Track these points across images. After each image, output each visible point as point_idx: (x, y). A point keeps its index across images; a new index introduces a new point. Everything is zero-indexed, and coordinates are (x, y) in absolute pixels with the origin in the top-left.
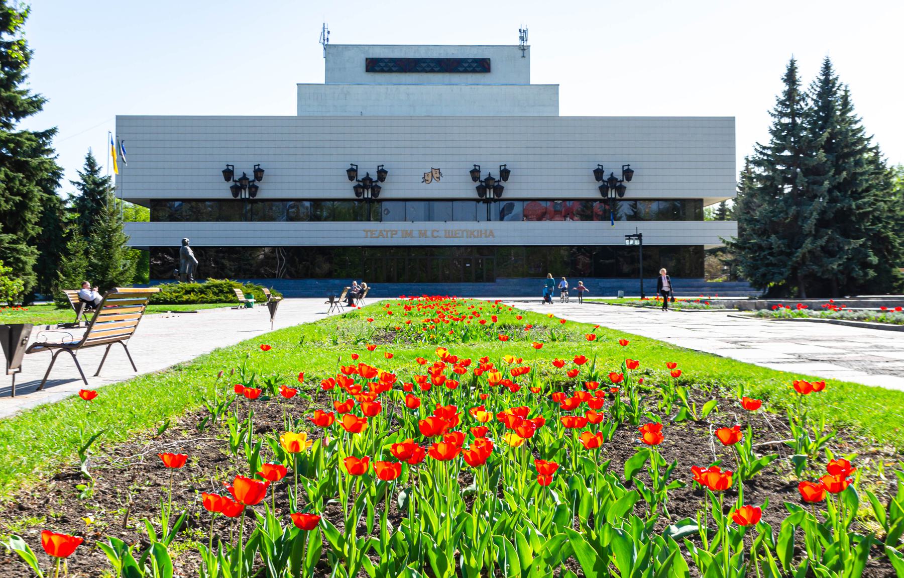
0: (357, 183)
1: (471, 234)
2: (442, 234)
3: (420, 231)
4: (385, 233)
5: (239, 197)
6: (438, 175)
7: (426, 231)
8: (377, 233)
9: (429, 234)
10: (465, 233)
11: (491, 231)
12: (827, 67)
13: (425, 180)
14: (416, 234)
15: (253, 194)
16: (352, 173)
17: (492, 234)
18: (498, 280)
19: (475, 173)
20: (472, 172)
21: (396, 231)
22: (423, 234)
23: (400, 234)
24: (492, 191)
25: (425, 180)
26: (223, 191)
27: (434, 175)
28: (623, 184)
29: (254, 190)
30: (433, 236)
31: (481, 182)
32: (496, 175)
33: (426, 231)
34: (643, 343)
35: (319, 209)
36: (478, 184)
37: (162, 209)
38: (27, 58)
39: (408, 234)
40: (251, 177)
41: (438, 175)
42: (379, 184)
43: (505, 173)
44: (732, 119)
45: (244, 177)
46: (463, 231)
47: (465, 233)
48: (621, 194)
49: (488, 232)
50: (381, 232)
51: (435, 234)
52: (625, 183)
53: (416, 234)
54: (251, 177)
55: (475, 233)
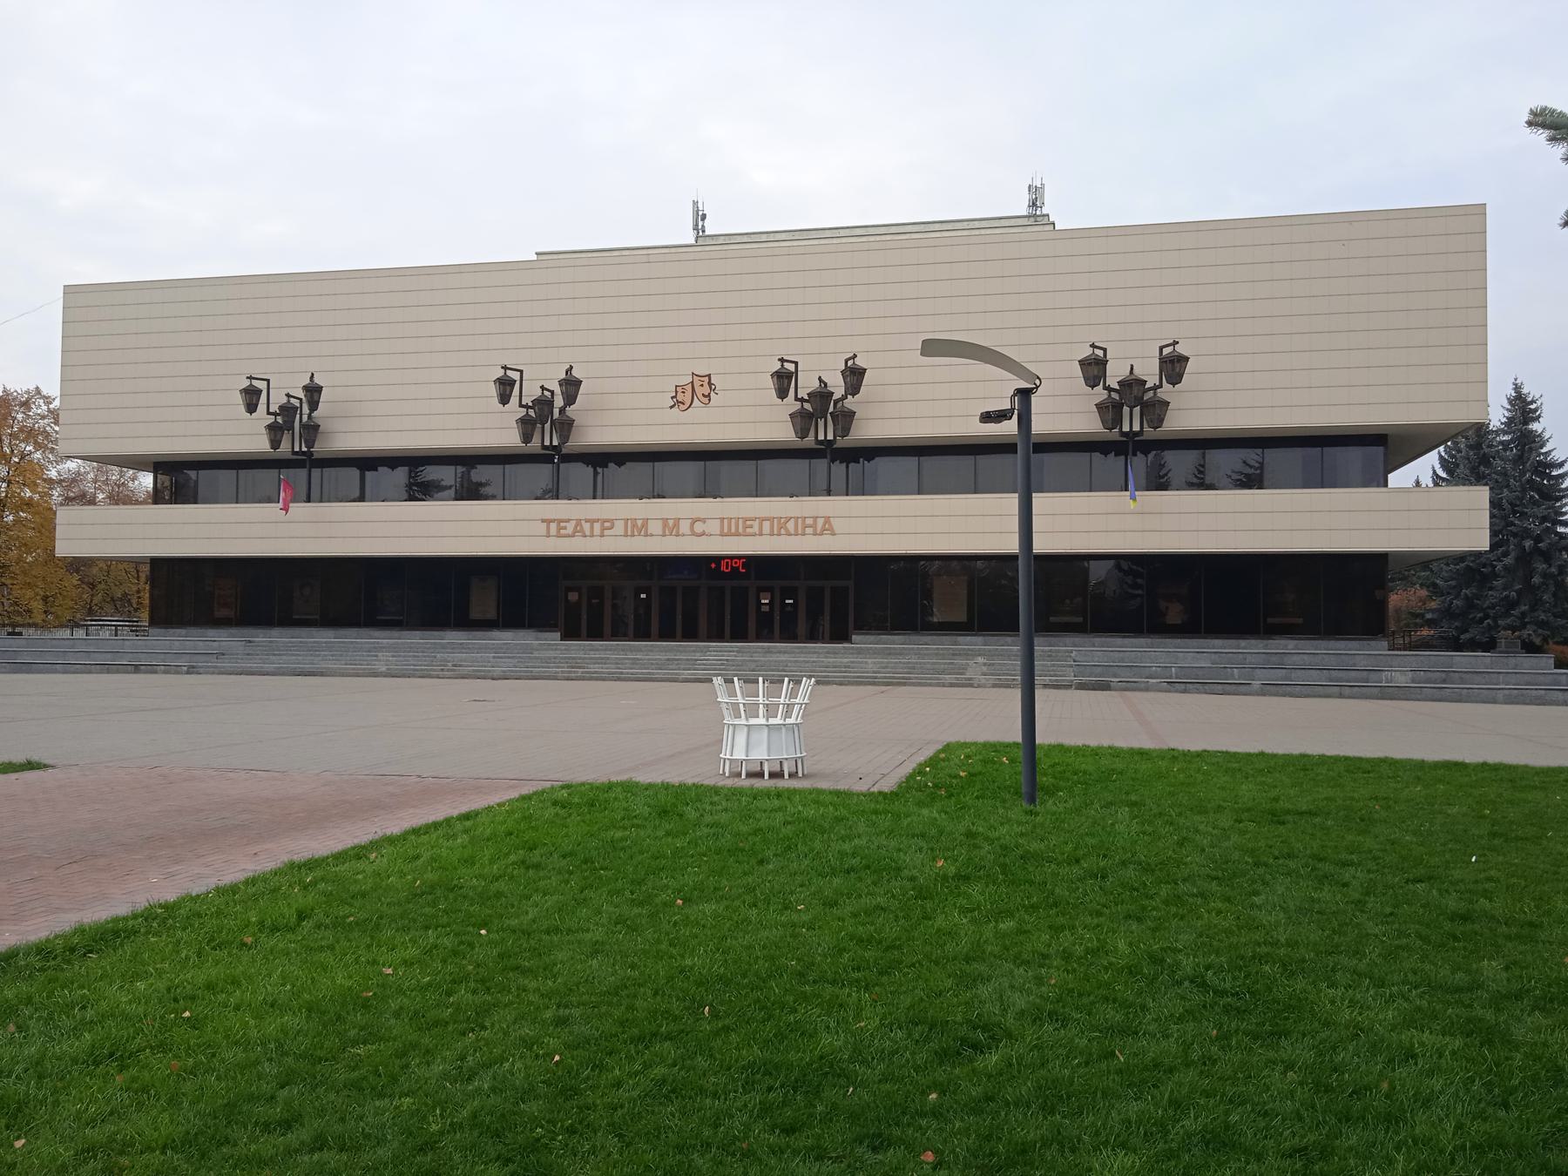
0: (798, 405)
4: (587, 526)
5: (811, 437)
6: (706, 390)
8: (570, 527)
9: (685, 527)
10: (766, 525)
12: (695, 203)
13: (677, 403)
15: (565, 438)
17: (828, 529)
21: (612, 521)
23: (619, 528)
24: (1137, 410)
25: (677, 403)
26: (250, 437)
27: (698, 390)
28: (1161, 394)
30: (694, 534)
31: (1109, 389)
32: (1149, 371)
34: (459, 826)
35: (420, 474)
36: (1100, 394)
37: (181, 479)
39: (638, 528)
40: (837, 386)
41: (706, 390)
42: (850, 402)
44: (1478, 212)
46: (592, 522)
47: (766, 525)
49: (820, 522)
50: (579, 522)
51: (699, 527)
54: (837, 386)
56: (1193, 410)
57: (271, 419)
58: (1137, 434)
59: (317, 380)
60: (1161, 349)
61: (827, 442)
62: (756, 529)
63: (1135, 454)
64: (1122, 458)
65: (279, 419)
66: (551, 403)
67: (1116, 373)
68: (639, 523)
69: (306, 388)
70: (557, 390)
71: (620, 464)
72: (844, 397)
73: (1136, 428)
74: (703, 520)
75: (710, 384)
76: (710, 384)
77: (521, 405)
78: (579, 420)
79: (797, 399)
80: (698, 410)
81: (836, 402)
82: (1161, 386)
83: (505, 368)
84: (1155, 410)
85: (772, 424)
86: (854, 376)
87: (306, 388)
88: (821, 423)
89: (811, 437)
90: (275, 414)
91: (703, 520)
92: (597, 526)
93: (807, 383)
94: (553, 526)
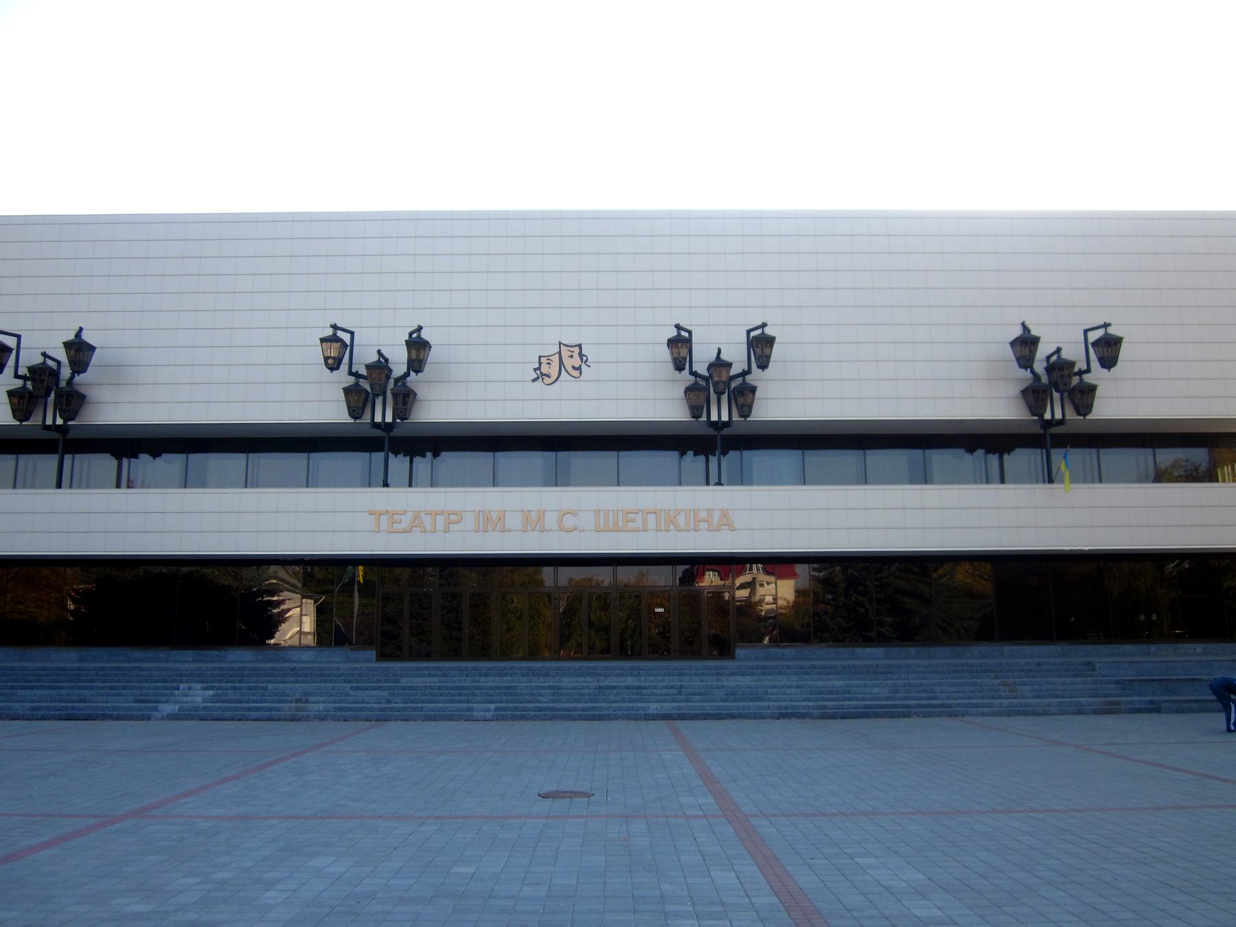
1: (667, 521)
2: (587, 520)
3: (526, 515)
4: (427, 520)
5: (366, 419)
6: (576, 361)
7: (542, 514)
8: (406, 521)
9: (551, 521)
10: (651, 519)
11: (725, 513)
13: (540, 375)
14: (514, 521)
16: (337, 348)
17: (725, 522)
18: (738, 651)
19: (337, 348)
20: (672, 343)
22: (533, 522)
23: (469, 521)
25: (540, 375)
27: (568, 361)
29: (743, 394)
30: (562, 529)
32: (737, 355)
33: (542, 514)
38: (690, 333)
40: (399, 359)
41: (576, 361)
43: (761, 345)
45: (719, 364)
47: (652, 518)
48: (746, 410)
49: (716, 516)
50: (417, 516)
51: (569, 521)
52: (1097, 375)
53: (514, 521)
55: (681, 520)
56: (781, 401)
57: (19, 383)
58: (727, 424)
59: (86, 337)
60: (749, 332)
61: (388, 427)
62: (639, 524)
63: (724, 453)
64: (702, 458)
65: (29, 385)
66: (55, 374)
67: (702, 357)
68: (534, 515)
69: (68, 345)
70: (61, 355)
71: (155, 455)
72: (407, 375)
73: (725, 418)
74: (574, 514)
75: (581, 355)
76: (581, 355)
77: (17, 376)
78: (93, 394)
79: (351, 373)
80: (567, 385)
81: (397, 380)
82: (749, 372)
83: (335, 327)
84: (1084, 396)
85: (663, 405)
86: (761, 345)
87: (68, 345)
88: (379, 401)
89: (704, 419)
90: (24, 378)
91: (574, 514)
92: (440, 520)
93: (365, 356)
94: (384, 519)
